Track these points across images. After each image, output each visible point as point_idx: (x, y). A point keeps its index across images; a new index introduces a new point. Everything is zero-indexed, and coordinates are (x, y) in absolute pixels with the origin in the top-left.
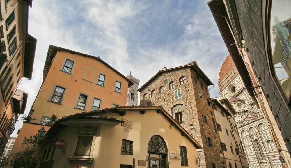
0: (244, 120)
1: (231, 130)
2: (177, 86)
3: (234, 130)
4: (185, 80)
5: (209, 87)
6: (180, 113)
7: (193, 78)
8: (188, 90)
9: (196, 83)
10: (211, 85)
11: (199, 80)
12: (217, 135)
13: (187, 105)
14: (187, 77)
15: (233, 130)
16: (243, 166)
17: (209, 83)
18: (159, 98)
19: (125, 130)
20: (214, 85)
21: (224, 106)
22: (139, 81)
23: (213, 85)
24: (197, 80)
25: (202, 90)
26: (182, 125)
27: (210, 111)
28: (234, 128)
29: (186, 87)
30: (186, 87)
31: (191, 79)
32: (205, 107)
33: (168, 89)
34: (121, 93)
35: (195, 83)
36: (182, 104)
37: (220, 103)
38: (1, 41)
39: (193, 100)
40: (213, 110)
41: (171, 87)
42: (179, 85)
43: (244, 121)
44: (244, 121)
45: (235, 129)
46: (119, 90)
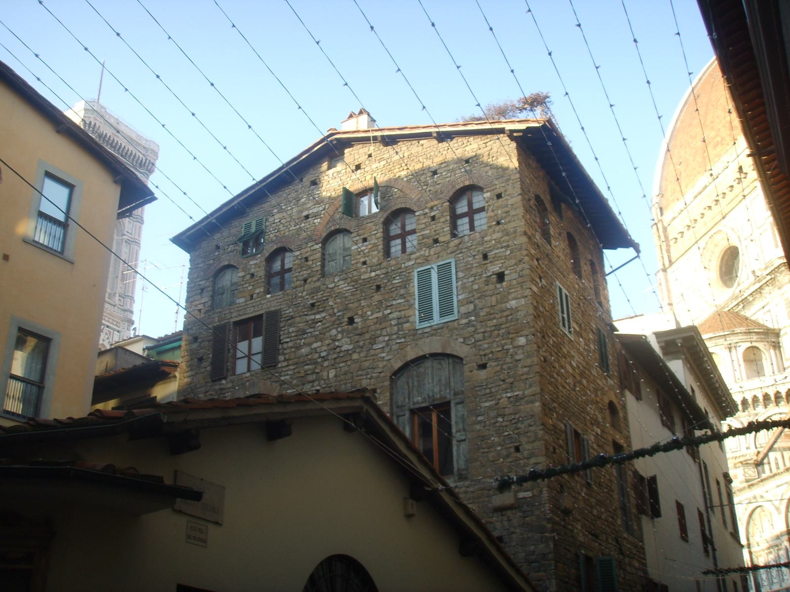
0: (771, 449)
1: (703, 509)
2: (436, 241)
3: (717, 510)
4: (482, 210)
5: (612, 257)
6: (444, 408)
7: (532, 202)
8: (501, 277)
9: (546, 235)
10: (620, 251)
11: (561, 217)
12: (631, 539)
13: (483, 366)
14: (499, 196)
15: (712, 507)
16: (72, 215)
17: (611, 233)
18: (313, 305)
19: (188, 537)
20: (638, 250)
21: (677, 367)
22: (156, 154)
23: (630, 252)
24: (552, 218)
25: (572, 276)
26: (451, 482)
27: (607, 401)
28: (716, 501)
29: (485, 257)
30: (485, 257)
31: (521, 211)
32: (584, 382)
33: (376, 257)
34: (68, 254)
35: (538, 236)
36: (457, 359)
37: (661, 355)
38: (152, 385)
39: (522, 341)
40: (623, 395)
41: (396, 246)
42: (445, 237)
43: (766, 455)
44: (766, 455)
45: (722, 505)
46: (59, 231)
